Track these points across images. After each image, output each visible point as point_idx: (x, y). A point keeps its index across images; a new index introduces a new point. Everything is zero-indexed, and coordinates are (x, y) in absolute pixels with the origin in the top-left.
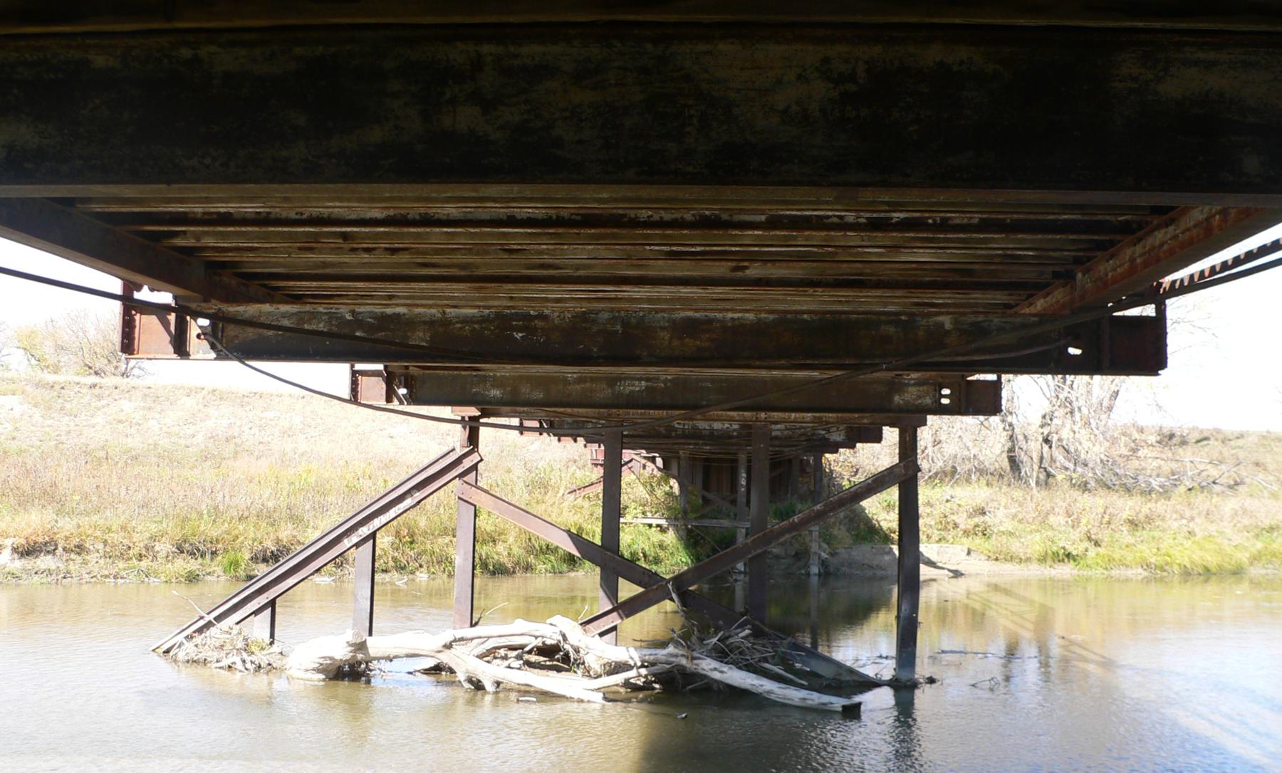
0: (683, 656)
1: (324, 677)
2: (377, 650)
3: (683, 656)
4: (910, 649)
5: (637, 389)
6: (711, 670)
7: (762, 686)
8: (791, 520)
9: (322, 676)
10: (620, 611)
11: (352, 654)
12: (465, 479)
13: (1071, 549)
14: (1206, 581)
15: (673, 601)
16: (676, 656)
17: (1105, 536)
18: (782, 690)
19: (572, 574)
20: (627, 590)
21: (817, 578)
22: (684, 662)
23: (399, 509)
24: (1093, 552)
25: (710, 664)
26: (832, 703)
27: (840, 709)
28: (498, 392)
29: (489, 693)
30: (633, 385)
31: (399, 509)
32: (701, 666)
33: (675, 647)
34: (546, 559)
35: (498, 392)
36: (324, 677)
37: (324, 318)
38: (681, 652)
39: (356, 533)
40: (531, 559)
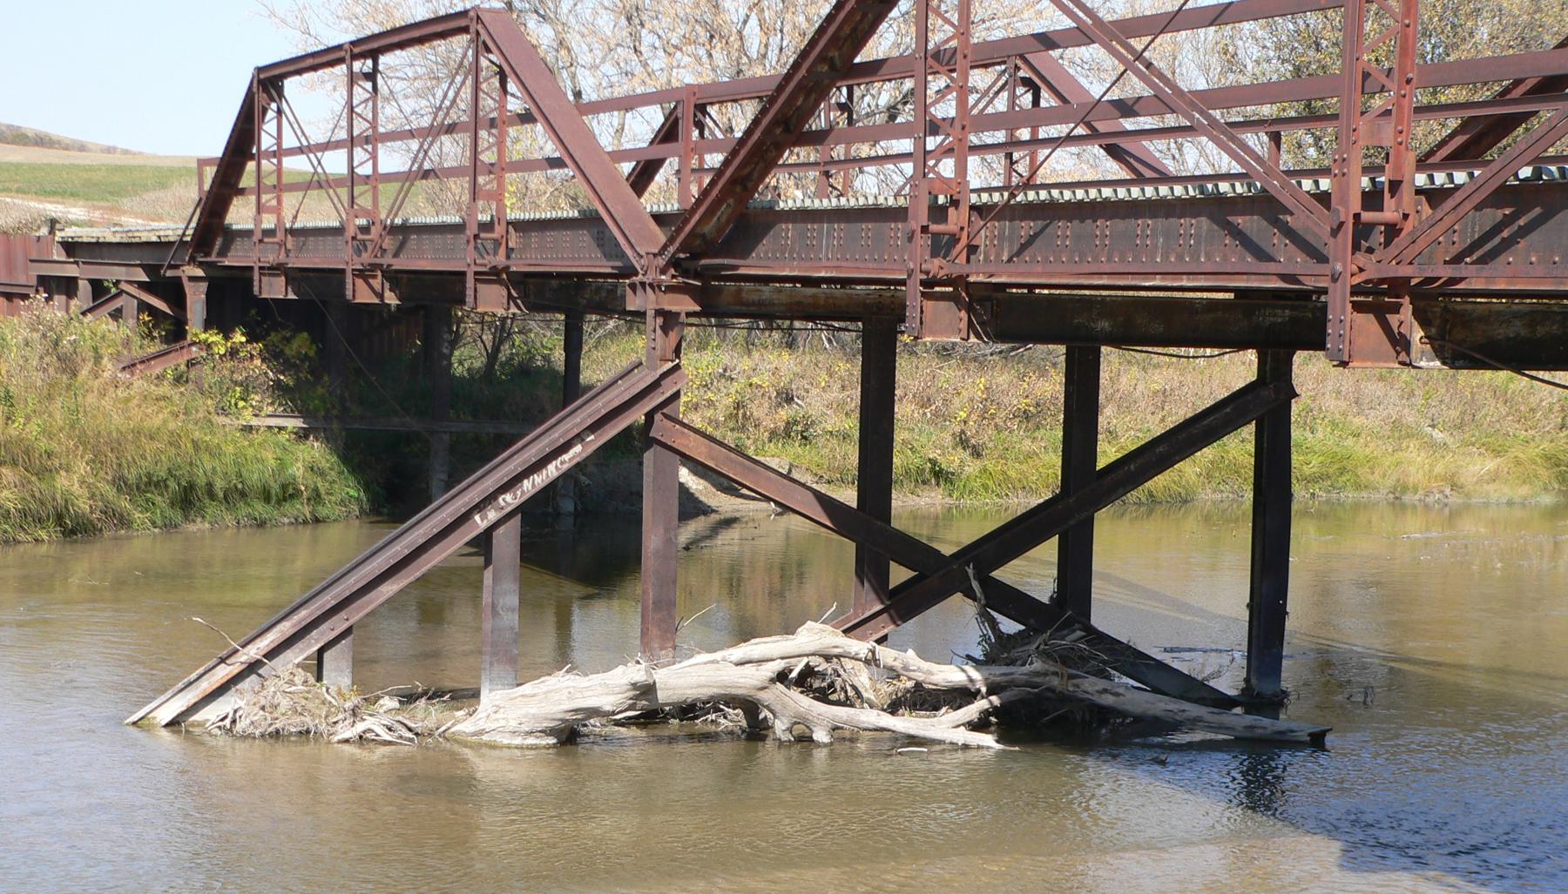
0: (1056, 674)
1: (555, 741)
2: (671, 692)
3: (1056, 674)
4: (1275, 651)
5: (1279, 320)
6: (1098, 692)
7: (1184, 711)
8: (1126, 468)
9: (552, 741)
10: (892, 611)
11: (631, 702)
12: (665, 411)
13: (944, 464)
14: (1150, 512)
15: (974, 598)
16: (1045, 674)
17: (987, 437)
18: (1216, 716)
19: (192, 528)
20: (899, 574)
21: (571, 520)
22: (1055, 682)
23: (562, 463)
24: (972, 467)
25: (1096, 684)
26: (1292, 731)
27: (1308, 738)
28: (1107, 324)
29: (819, 745)
30: (1274, 316)
31: (562, 463)
32: (1082, 687)
33: (1044, 662)
34: (147, 500)
35: (1107, 324)
36: (555, 741)
37: (1558, 318)
38: (1052, 669)
39: (494, 504)
40: (124, 503)
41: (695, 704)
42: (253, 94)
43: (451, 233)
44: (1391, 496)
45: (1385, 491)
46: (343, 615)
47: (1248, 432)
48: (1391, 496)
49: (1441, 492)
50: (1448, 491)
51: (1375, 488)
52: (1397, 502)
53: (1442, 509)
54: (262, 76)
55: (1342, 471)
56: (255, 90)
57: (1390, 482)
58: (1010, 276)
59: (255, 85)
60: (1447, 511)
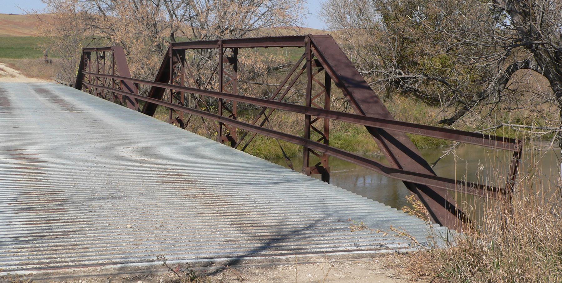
41: (448, 125)
42: (169, 58)
43: (255, 128)
44: (363, 153)
45: (362, 152)
46: (262, 232)
47: (311, 121)
48: (363, 153)
49: (377, 152)
50: (379, 152)
51: (358, 151)
52: (365, 155)
53: (377, 158)
54: (174, 48)
55: (348, 145)
56: (171, 56)
57: (363, 149)
58: (283, 44)
59: (170, 52)
60: (379, 158)
